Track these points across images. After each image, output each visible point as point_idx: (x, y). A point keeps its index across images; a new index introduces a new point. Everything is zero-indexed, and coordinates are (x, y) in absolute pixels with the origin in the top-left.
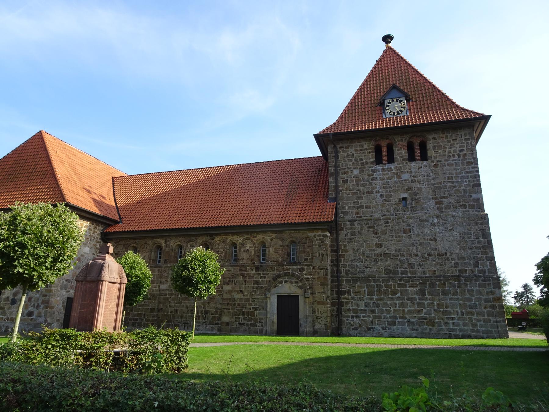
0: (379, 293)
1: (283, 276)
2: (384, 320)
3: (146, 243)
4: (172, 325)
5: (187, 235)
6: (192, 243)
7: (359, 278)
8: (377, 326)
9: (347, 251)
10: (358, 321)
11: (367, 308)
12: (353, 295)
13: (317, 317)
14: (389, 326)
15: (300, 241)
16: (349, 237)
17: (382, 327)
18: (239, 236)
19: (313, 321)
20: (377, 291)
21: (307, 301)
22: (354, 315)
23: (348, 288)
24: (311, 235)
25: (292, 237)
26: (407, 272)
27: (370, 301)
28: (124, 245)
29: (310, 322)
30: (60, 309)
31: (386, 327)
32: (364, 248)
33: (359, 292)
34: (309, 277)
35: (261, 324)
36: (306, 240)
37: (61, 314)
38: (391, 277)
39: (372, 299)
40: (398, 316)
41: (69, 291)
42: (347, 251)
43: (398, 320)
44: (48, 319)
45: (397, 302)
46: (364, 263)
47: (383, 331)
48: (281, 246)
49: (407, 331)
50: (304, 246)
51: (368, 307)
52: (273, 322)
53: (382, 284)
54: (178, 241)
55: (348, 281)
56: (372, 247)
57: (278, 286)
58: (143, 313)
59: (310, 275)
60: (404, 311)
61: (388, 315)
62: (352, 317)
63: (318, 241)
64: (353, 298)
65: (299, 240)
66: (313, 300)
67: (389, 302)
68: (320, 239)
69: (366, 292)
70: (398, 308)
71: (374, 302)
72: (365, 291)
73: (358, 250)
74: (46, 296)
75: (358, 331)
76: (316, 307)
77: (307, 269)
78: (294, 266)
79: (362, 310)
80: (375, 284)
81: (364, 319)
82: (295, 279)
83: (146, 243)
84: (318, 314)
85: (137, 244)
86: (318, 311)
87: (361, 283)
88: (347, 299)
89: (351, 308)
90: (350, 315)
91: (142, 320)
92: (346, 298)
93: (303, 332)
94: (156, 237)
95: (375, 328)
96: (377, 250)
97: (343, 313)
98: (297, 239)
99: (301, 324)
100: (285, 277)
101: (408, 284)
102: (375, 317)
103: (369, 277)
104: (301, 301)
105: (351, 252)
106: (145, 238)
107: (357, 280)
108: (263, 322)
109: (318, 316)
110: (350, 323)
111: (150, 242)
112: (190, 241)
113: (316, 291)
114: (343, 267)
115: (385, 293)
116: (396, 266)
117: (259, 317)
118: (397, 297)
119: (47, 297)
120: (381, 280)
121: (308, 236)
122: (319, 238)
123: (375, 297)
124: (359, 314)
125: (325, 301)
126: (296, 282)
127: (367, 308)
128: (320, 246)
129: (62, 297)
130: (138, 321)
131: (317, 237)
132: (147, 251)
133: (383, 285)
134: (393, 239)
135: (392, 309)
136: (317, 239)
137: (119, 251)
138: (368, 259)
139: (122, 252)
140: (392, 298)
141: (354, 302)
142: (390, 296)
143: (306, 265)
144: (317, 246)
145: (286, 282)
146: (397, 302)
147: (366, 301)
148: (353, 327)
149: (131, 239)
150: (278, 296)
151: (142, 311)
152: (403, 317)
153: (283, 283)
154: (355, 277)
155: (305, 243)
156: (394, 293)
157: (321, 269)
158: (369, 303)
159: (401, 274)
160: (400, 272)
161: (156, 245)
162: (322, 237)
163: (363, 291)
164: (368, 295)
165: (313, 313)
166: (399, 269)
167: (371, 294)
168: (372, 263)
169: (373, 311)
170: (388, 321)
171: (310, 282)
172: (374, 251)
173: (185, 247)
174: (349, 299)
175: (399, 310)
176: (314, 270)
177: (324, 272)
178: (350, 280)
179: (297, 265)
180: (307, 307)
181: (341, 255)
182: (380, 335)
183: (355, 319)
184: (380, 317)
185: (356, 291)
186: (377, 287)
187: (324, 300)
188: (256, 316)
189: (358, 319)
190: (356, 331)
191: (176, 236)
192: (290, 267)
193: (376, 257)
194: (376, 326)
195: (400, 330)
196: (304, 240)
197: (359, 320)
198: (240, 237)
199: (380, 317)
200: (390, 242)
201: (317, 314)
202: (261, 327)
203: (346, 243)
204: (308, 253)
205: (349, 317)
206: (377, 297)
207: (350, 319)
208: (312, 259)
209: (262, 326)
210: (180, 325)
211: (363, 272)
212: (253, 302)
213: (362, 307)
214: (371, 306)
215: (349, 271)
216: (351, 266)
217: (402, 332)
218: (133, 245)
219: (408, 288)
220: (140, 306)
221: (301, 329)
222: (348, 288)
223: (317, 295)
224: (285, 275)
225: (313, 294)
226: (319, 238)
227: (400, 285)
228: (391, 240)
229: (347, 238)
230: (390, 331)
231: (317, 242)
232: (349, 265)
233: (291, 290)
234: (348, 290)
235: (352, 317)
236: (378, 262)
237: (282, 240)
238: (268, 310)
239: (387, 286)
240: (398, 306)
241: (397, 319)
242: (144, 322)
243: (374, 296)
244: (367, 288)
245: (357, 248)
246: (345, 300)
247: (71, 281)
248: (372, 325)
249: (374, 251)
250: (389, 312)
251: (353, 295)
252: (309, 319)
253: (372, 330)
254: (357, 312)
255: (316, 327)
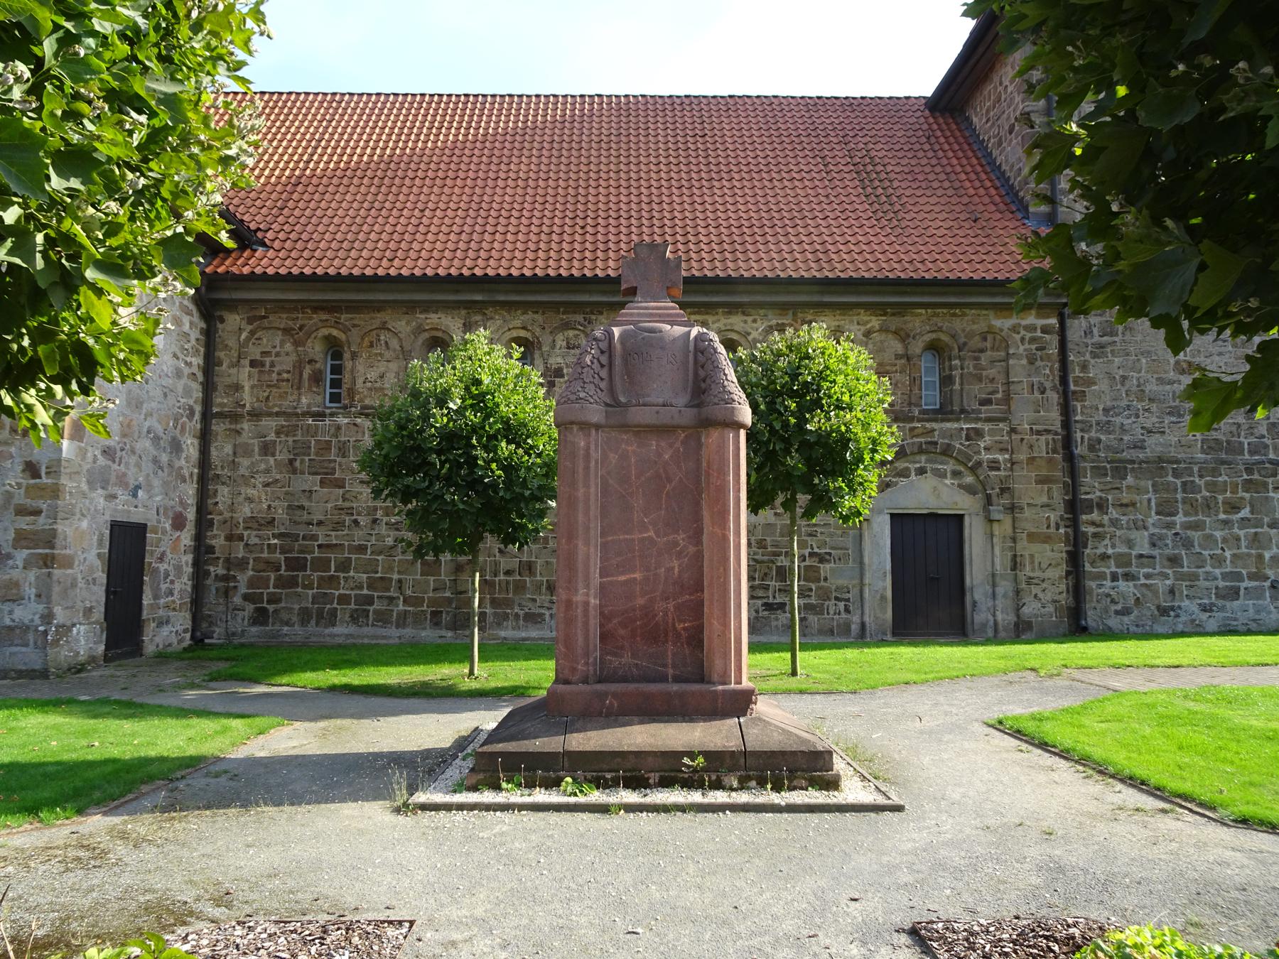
0: (1192, 506)
1: (913, 454)
2: (1207, 584)
3: (383, 327)
4: (517, 615)
5: (555, 306)
6: (571, 333)
7: (1133, 462)
8: (1186, 603)
9: (1091, 382)
10: (1132, 589)
11: (1156, 552)
12: (1114, 513)
13: (1030, 580)
14: (1220, 603)
15: (965, 344)
16: (1096, 339)
17: (1200, 605)
18: (750, 319)
19: (1017, 592)
20: (1184, 501)
21: (997, 533)
22: (1120, 571)
23: (1098, 494)
24: (1003, 323)
25: (940, 329)
26: (1266, 446)
27: (1164, 531)
28: (287, 331)
29: (1005, 596)
30: (92, 569)
31: (1212, 604)
32: (1143, 374)
33: (1133, 504)
34: (1000, 457)
35: (841, 605)
36: (985, 339)
37: (95, 588)
38: (1223, 462)
39: (1170, 526)
40: (1244, 572)
41: (114, 497)
42: (1091, 382)
43: (1243, 585)
44: (58, 610)
45: (1242, 533)
46: (1141, 419)
47: (1204, 616)
48: (898, 357)
49: (1270, 613)
50: (977, 359)
51: (1160, 548)
52: (883, 598)
53: (1197, 480)
54: (518, 323)
55: (1099, 472)
56: (1166, 372)
57: (896, 484)
58: (395, 577)
59: (1003, 450)
60: (1260, 557)
61: (1217, 572)
62: (1114, 577)
63: (1027, 346)
64: (1114, 523)
65: (963, 340)
66: (1014, 528)
67: (1218, 534)
68: (1032, 340)
69: (1153, 504)
70: (1244, 550)
71: (1176, 534)
72: (1149, 500)
73: (1124, 378)
74: (37, 513)
75: (1132, 617)
76: (1025, 548)
77: (992, 433)
78: (949, 420)
79: (1141, 556)
80: (1178, 482)
81: (1148, 582)
82: (952, 461)
83: (383, 327)
84: (1033, 570)
85: (345, 330)
86: (1032, 562)
87: (1136, 478)
88: (1098, 526)
89: (1110, 551)
90: (1108, 571)
91: (391, 599)
92: (1093, 523)
93: (984, 625)
94: (428, 307)
95: (1179, 607)
96: (1179, 382)
97: (1088, 567)
98: (953, 336)
99: (974, 604)
100: (918, 457)
101: (1270, 480)
102: (1180, 577)
103: (1160, 459)
104: (974, 533)
105: (1103, 385)
106: (379, 307)
107: (1126, 468)
108: (848, 600)
109: (1031, 578)
110: (1108, 595)
111: (403, 325)
112: (566, 326)
113: (1024, 502)
114: (1082, 430)
115: (1208, 506)
116: (1234, 429)
117: (834, 583)
118: (1242, 519)
119: (41, 520)
120: (1196, 469)
121: (990, 326)
122: (1029, 335)
123: (1180, 519)
124: (1133, 569)
125: (1052, 530)
126: (956, 474)
127: (1156, 552)
128: (1031, 361)
129: (93, 518)
130: (377, 606)
131: (1023, 332)
132: (388, 354)
133: (1202, 483)
134: (1223, 349)
135: (1228, 554)
136: (1023, 339)
137: (264, 353)
138: (1154, 407)
139: (278, 355)
140: (1225, 522)
141: (1118, 533)
142: (1222, 516)
143: (988, 420)
144: (1024, 362)
145: (921, 471)
146: (1242, 533)
147: (1152, 530)
148: (1119, 607)
149: (318, 307)
150: (892, 515)
151: (391, 569)
152: (1258, 576)
153: (913, 477)
154: (1121, 461)
155: (982, 351)
156: (1234, 507)
157: (1039, 433)
158: (1161, 538)
159: (1250, 452)
160: (1246, 446)
161: (426, 335)
162: (1039, 334)
163: (1145, 503)
164: (1158, 513)
165: (1014, 568)
166: (1242, 439)
167: (1166, 509)
168: (1167, 420)
169: (1174, 561)
170: (1217, 588)
171: (1002, 473)
172: (1171, 383)
173: (545, 349)
174: (1102, 525)
175: (1249, 555)
176: (1014, 436)
177: (1047, 444)
178: (1105, 468)
179: (958, 420)
180: (997, 550)
181: (1074, 392)
182: (1198, 631)
183: (1122, 584)
184: (1193, 577)
185: (1125, 501)
186: (1184, 491)
187: (1048, 527)
188: (826, 579)
189: (1131, 584)
190: (1126, 619)
191: (509, 306)
192: (934, 425)
193: (1177, 403)
194: (1182, 600)
195: (1251, 611)
196: (976, 342)
197: (1135, 586)
198: (755, 321)
199: (1193, 577)
200: (1217, 358)
201: (1028, 571)
202: (844, 615)
203: (1088, 356)
204: (992, 380)
205: (1105, 579)
206: (1184, 519)
207: (1108, 583)
208: (1007, 399)
209: (847, 610)
210: (547, 613)
211: (1139, 446)
212: (810, 535)
213: (1142, 546)
214: (1166, 545)
215: (1099, 441)
216: (1105, 427)
217: (1257, 617)
218: (325, 332)
219: (1271, 494)
220: (380, 553)
221: (981, 617)
222: (1098, 494)
223: (1028, 513)
224: (921, 451)
225: (1012, 509)
226: (1029, 335)
227: (1248, 485)
228: (1220, 354)
229: (1089, 342)
230: (1221, 615)
231: (1022, 348)
232: (1098, 424)
233: (938, 497)
234: (1101, 498)
235: (1114, 577)
236: (1182, 416)
237: (904, 336)
238: (866, 560)
239: (1212, 487)
240: (1243, 543)
241: (1243, 581)
242: (401, 607)
243: (1174, 515)
244: (1155, 491)
245: (1121, 372)
246: (1091, 530)
247: (119, 454)
248: (1173, 600)
249: (1171, 383)
250: (1219, 561)
251: (1114, 513)
252: (1004, 587)
253: (1172, 613)
254: (1129, 564)
255: (1025, 610)
